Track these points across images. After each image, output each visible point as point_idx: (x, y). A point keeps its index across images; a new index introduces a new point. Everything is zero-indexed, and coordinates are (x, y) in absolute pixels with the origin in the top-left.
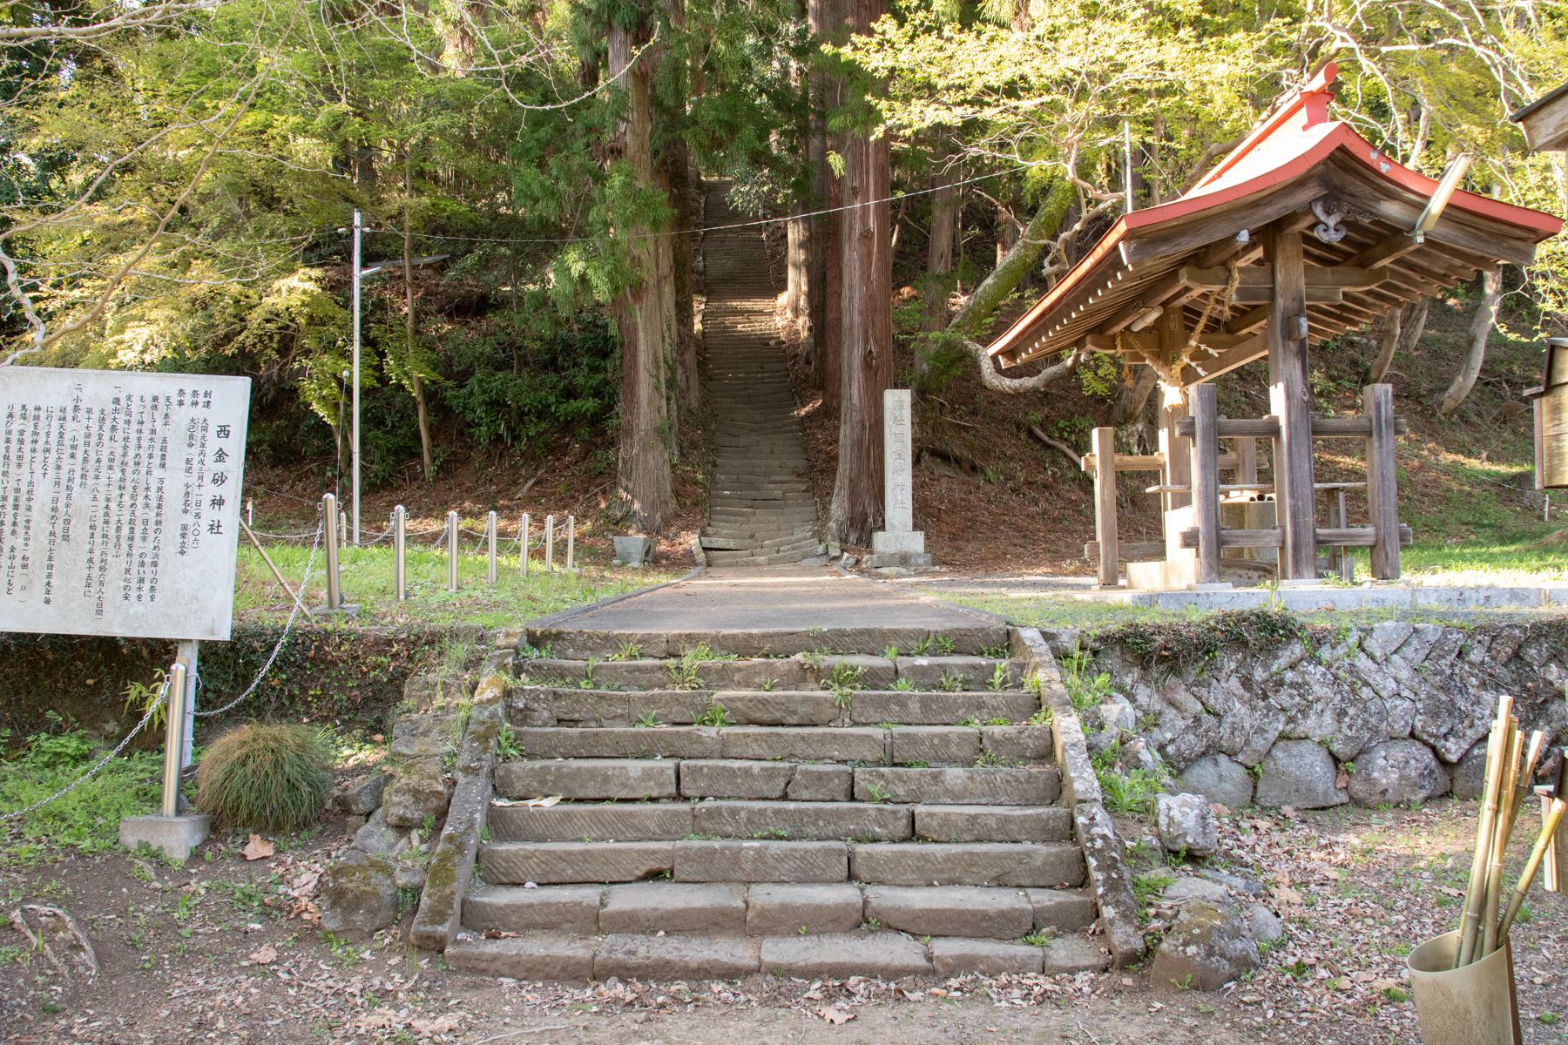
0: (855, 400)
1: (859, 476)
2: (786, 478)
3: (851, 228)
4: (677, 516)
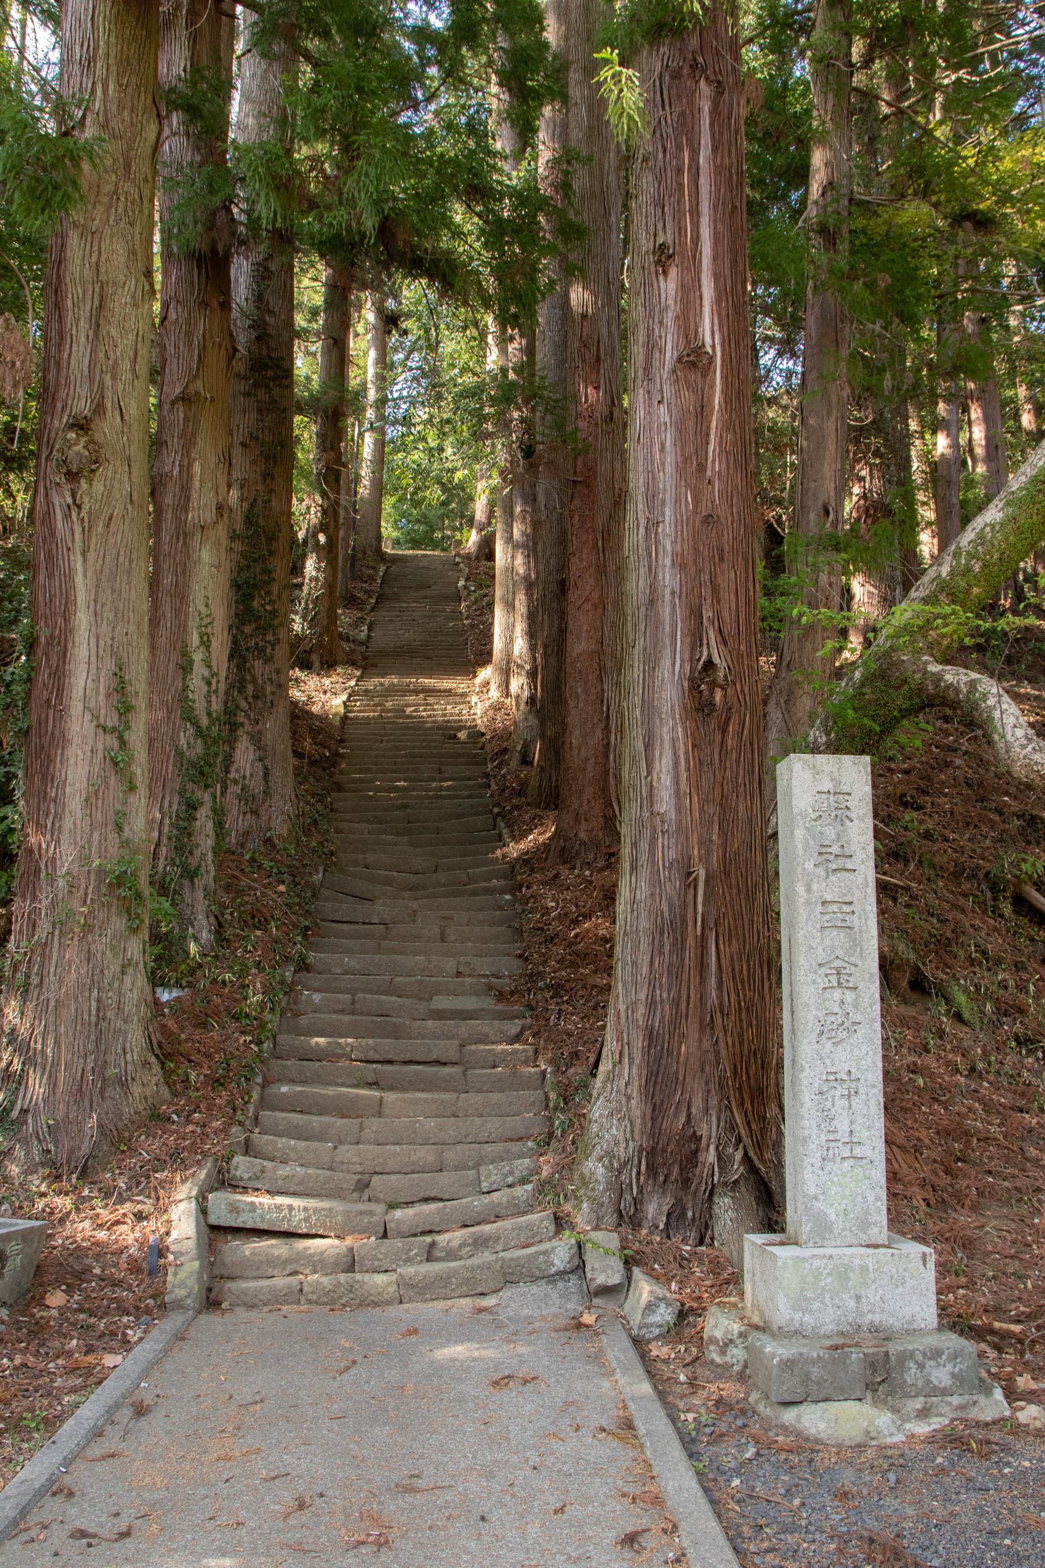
0: (665, 802)
1: (676, 1021)
2: (469, 1003)
3: (651, 346)
4: (157, 1118)
